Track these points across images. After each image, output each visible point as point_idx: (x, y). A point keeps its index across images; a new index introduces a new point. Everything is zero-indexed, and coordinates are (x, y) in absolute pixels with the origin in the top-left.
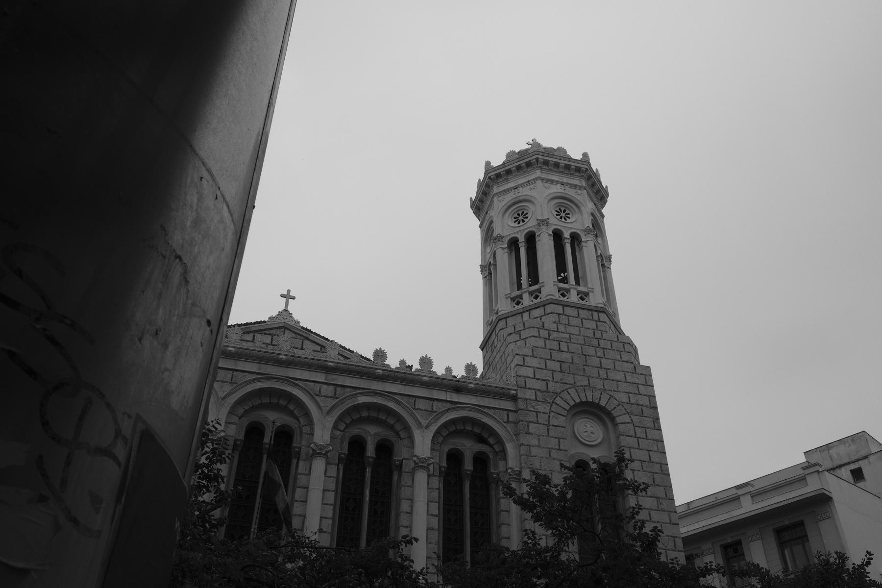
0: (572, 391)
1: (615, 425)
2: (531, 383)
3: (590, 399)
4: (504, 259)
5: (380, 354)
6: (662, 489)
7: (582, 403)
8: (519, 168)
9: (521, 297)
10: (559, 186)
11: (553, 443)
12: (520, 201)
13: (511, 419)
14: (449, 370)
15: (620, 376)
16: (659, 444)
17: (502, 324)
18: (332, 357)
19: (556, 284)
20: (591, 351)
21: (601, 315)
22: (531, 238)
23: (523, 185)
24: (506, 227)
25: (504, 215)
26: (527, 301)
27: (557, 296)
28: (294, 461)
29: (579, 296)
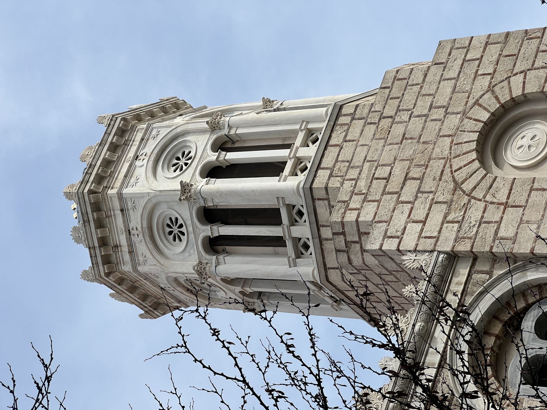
8: (100, 224)
12: (150, 229)
15: (447, 88)
19: (285, 227)
20: (398, 130)
21: (344, 111)
23: (126, 222)
27: (302, 177)
29: (310, 144)
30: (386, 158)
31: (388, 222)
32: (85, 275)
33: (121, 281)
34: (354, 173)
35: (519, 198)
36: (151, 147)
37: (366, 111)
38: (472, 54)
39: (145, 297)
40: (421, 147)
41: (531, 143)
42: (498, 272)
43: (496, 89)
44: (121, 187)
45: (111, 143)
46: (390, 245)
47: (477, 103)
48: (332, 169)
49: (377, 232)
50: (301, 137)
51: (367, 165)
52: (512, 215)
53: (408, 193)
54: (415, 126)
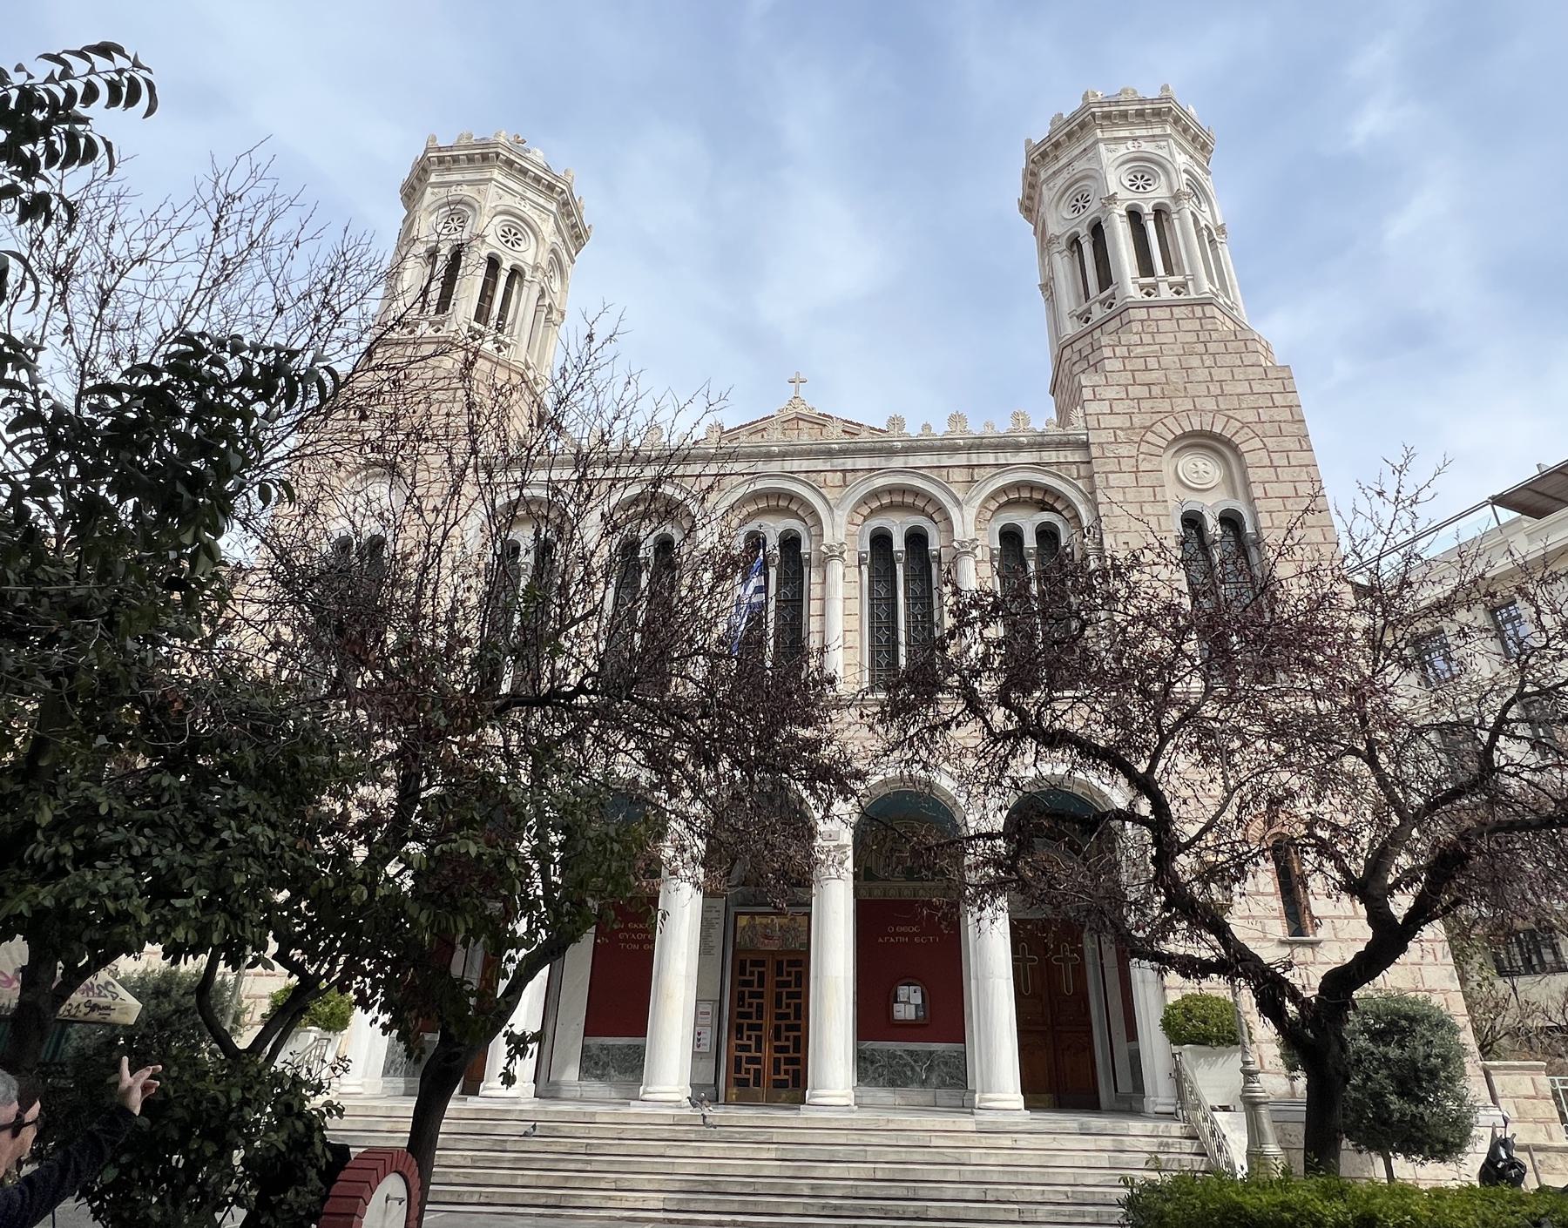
0: (1169, 421)
1: (1239, 456)
2: (1107, 421)
3: (1197, 427)
4: (1062, 265)
5: (896, 422)
6: (1317, 530)
7: (1185, 435)
8: (1070, 135)
9: (1089, 311)
10: (1130, 143)
11: (1147, 494)
12: (1077, 181)
13: (1082, 474)
14: (926, 427)
15: (1243, 388)
16: (1311, 469)
17: (1067, 352)
18: (834, 436)
20: (1195, 361)
21: (1207, 308)
22: (1097, 230)
24: (1061, 221)
25: (1057, 206)
26: (1098, 313)
27: (1139, 296)
28: (806, 570)
30: (1165, 361)
31: (1107, 384)
32: (1029, 142)
33: (1033, 174)
34: (1147, 338)
35: (1145, 480)
36: (1148, 147)
37: (1209, 327)
38: (1278, 399)
39: (1030, 198)
40: (1181, 387)
41: (1201, 472)
42: (1080, 484)
43: (1246, 429)
44: (1103, 140)
45: (1144, 110)
46: (1087, 393)
47: (1230, 417)
48: (1149, 319)
49: (1098, 379)
50: (1178, 279)
51: (1157, 347)
52: (1129, 479)
53: (1135, 391)
54: (1202, 374)
